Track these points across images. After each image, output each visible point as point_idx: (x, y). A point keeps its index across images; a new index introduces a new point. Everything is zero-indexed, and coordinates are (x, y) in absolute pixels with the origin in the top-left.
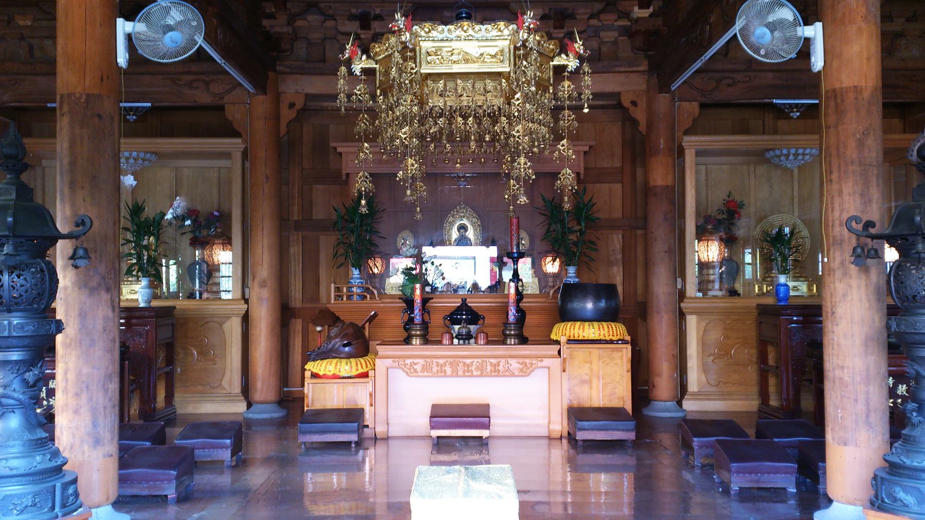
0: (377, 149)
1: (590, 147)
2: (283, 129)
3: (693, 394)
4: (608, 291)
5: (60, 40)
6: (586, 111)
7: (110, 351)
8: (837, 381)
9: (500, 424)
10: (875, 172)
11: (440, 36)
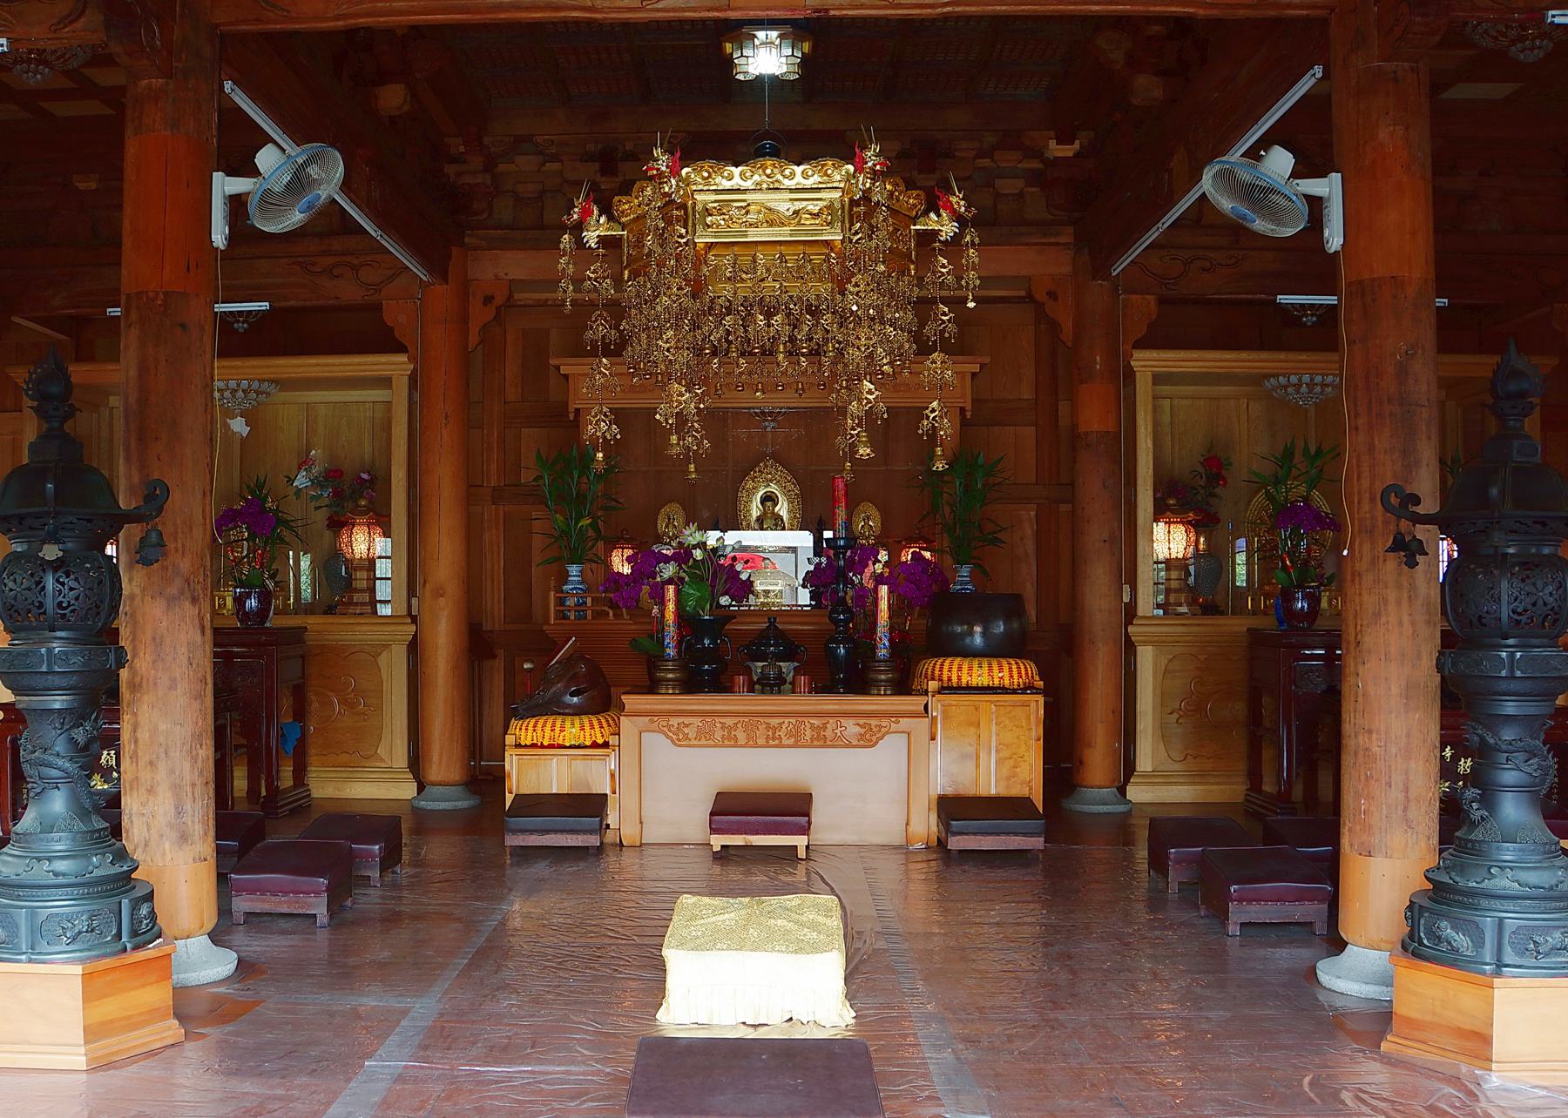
0: (623, 369)
1: (982, 366)
2: (473, 338)
3: (1145, 775)
4: (1012, 606)
5: (128, 210)
6: (971, 305)
7: (199, 696)
8: (1361, 753)
9: (832, 822)
10: (1425, 415)
11: (727, 184)
